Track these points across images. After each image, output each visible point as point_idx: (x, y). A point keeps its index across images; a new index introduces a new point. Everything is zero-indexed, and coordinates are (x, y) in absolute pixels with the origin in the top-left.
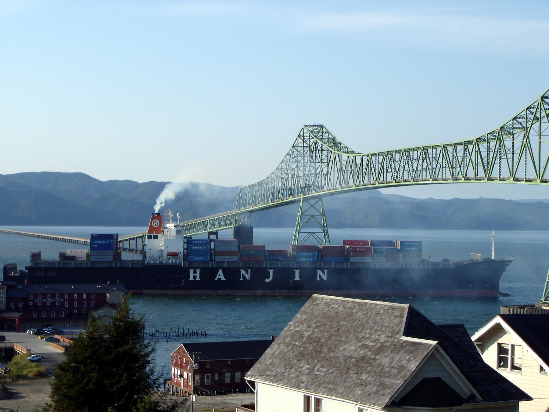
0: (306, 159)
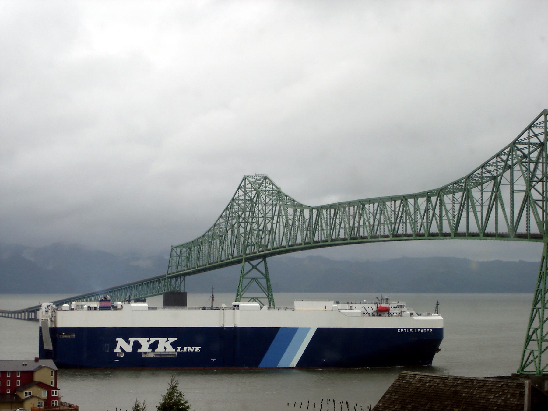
0: (247, 213)
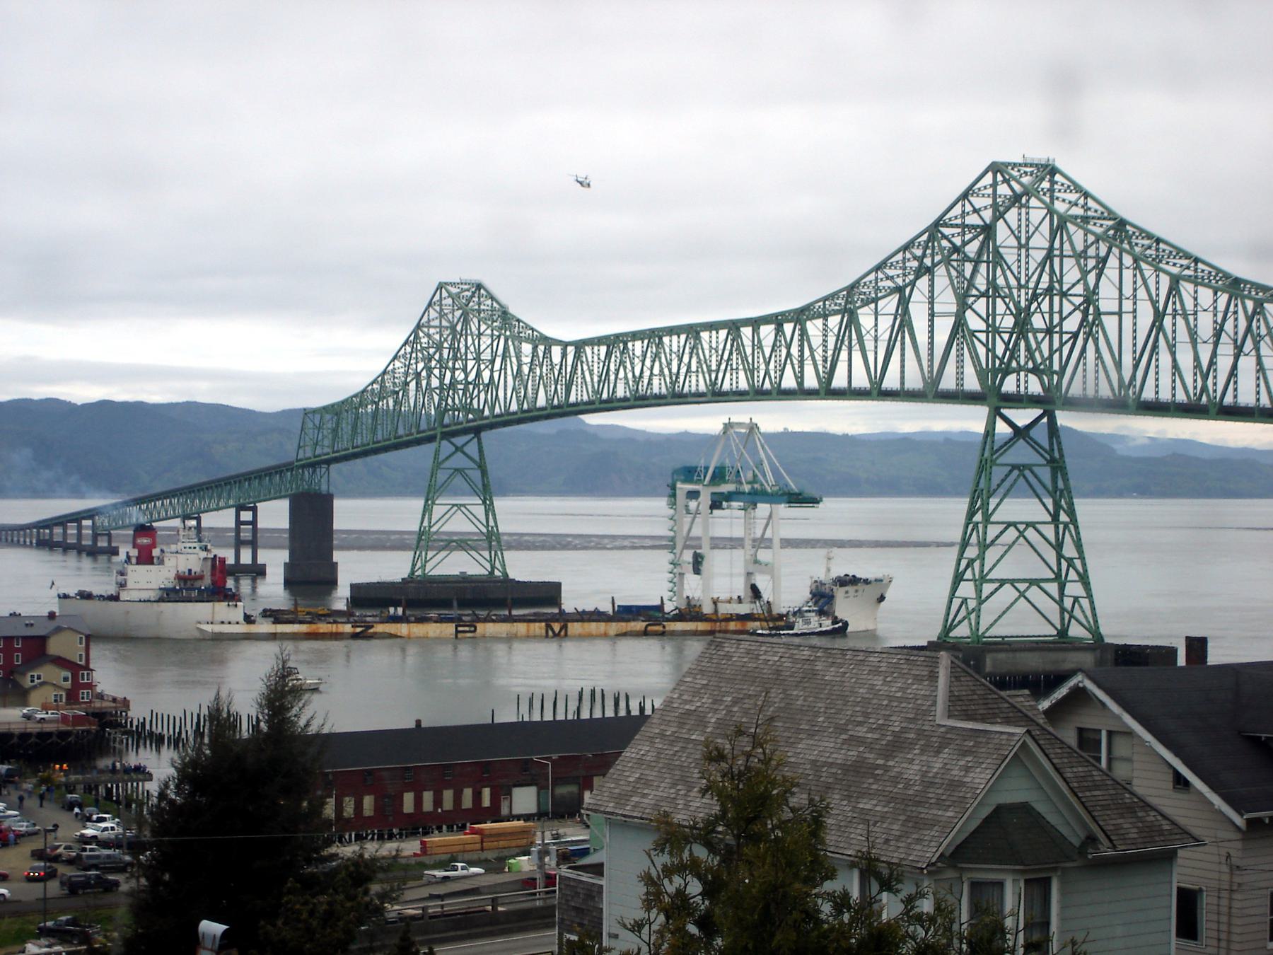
0: (445, 352)
